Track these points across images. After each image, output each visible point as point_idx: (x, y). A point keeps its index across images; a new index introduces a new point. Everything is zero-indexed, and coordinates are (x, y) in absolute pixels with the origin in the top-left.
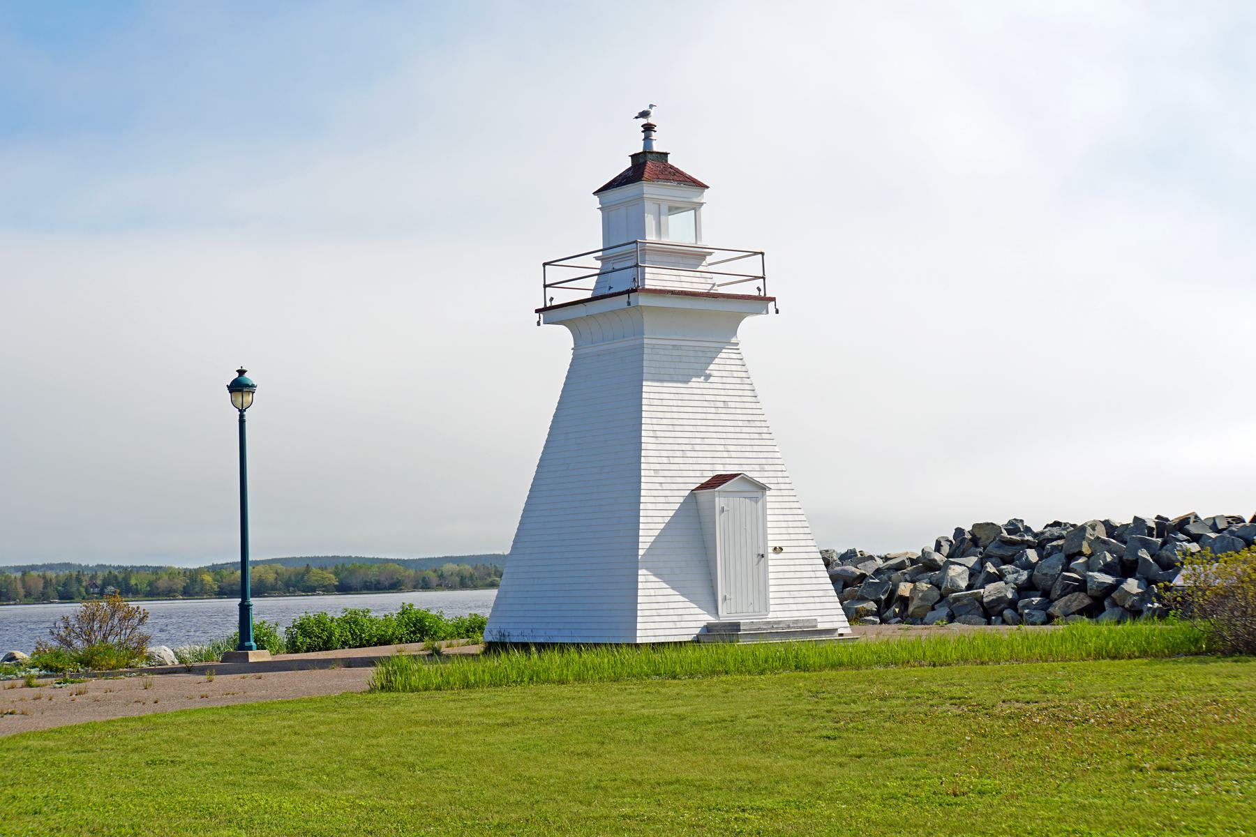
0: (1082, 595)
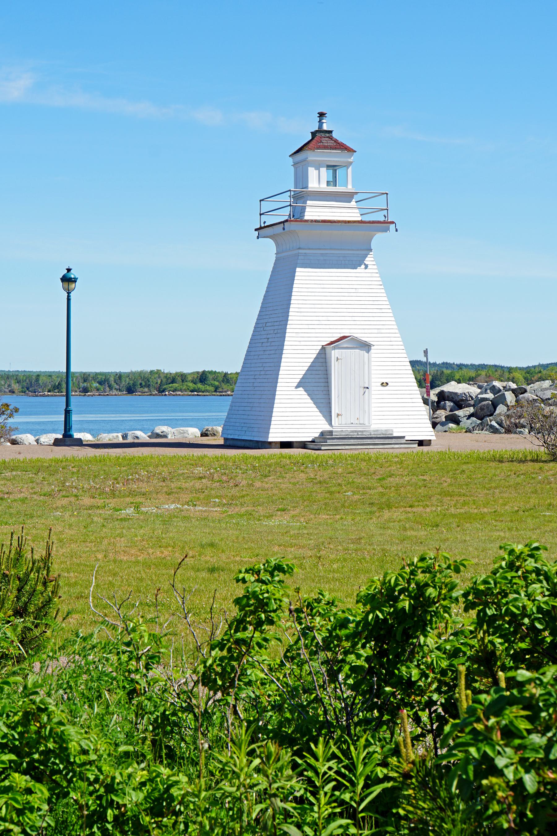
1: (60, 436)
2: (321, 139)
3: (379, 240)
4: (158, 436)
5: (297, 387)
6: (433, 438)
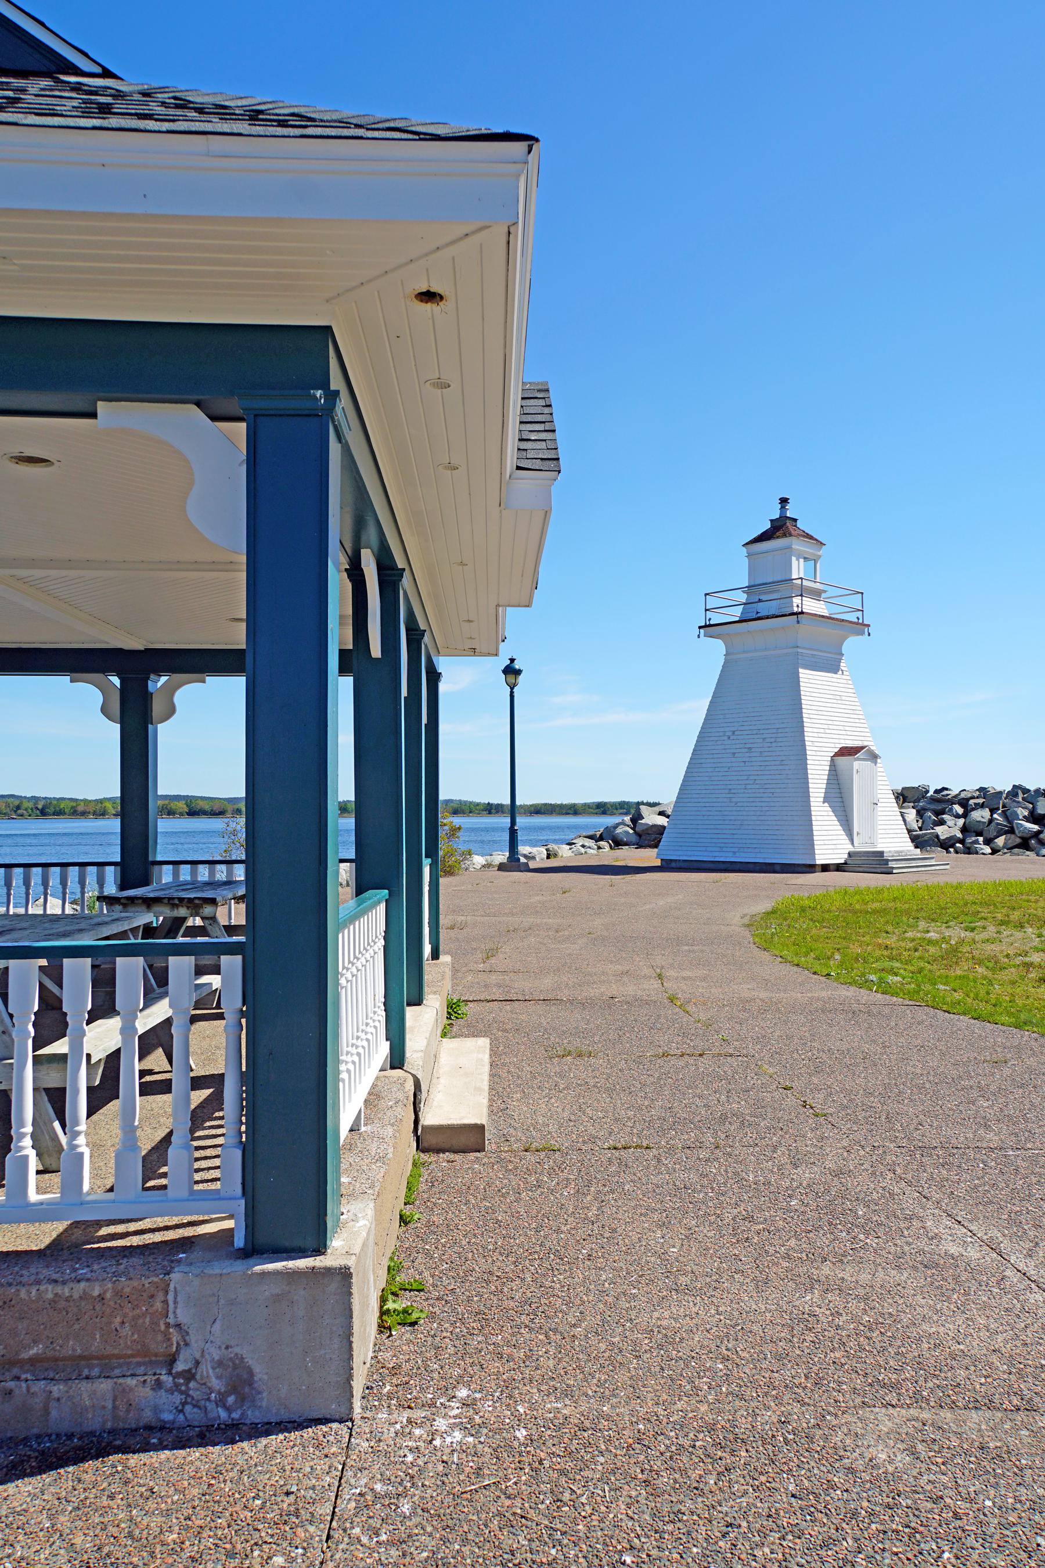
0: (1013, 836)
3: (852, 645)
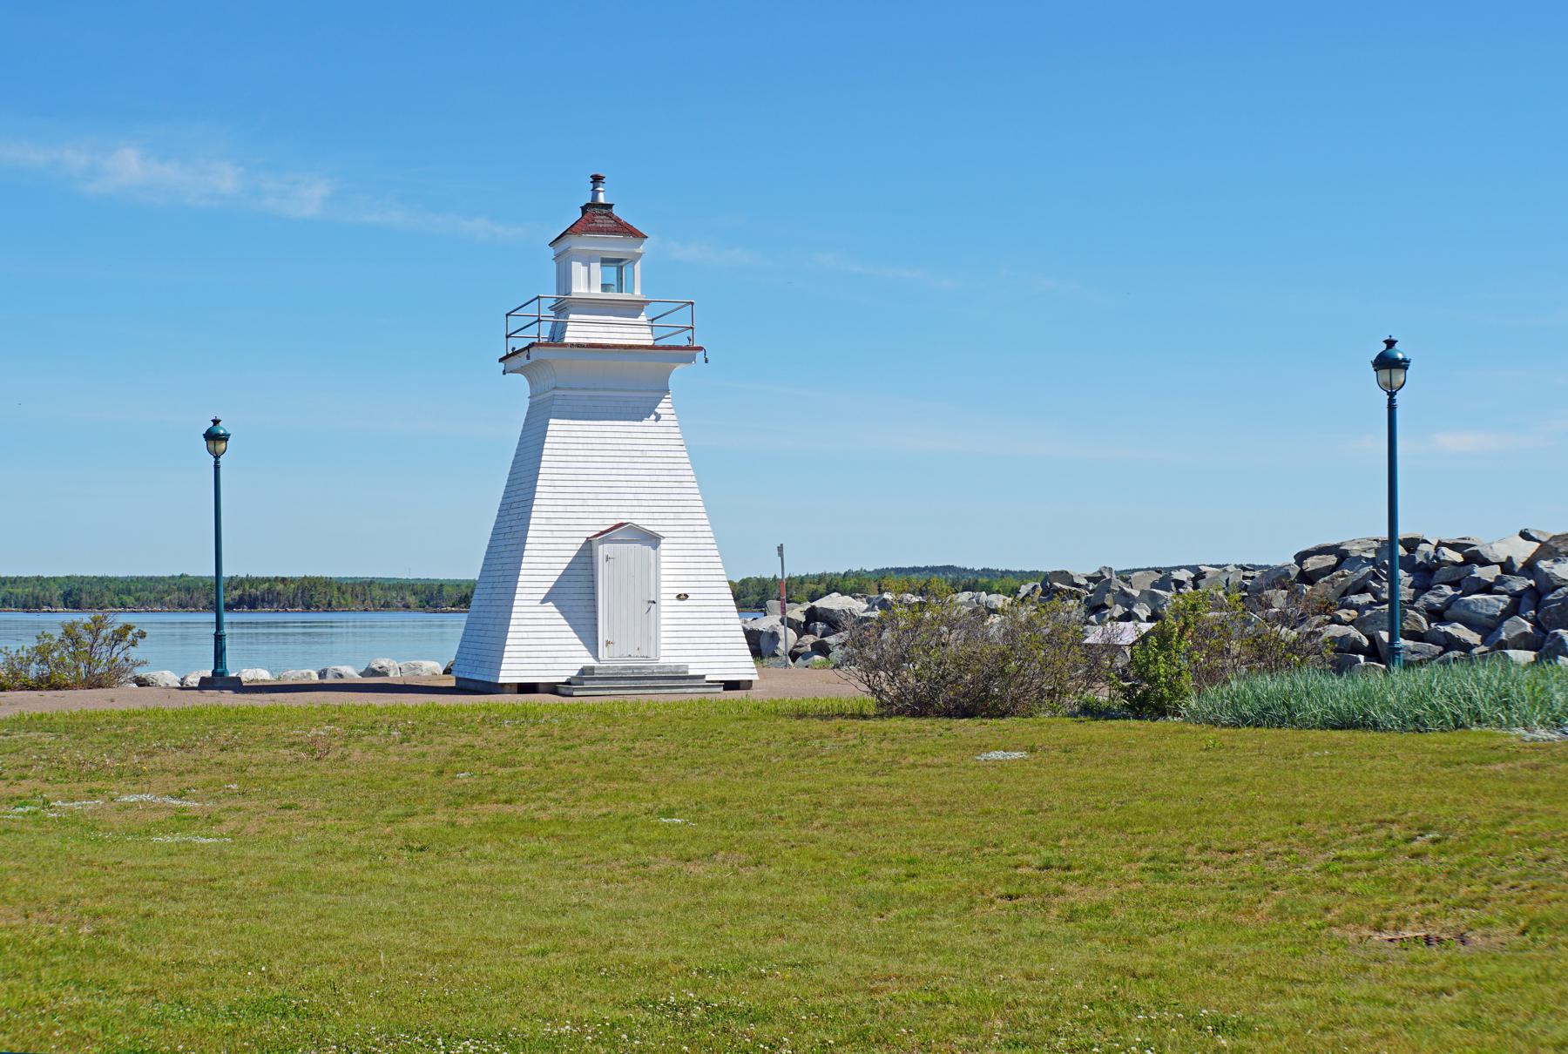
1: (209, 674)
2: (596, 218)
3: (680, 374)
4: (374, 673)
5: (543, 601)
6: (755, 678)
